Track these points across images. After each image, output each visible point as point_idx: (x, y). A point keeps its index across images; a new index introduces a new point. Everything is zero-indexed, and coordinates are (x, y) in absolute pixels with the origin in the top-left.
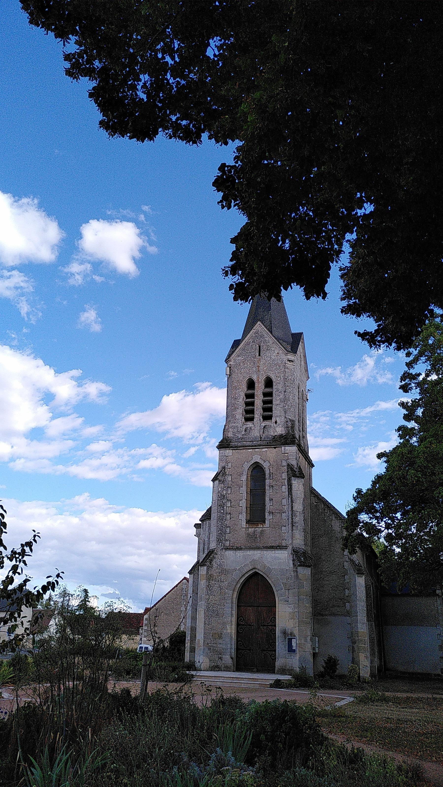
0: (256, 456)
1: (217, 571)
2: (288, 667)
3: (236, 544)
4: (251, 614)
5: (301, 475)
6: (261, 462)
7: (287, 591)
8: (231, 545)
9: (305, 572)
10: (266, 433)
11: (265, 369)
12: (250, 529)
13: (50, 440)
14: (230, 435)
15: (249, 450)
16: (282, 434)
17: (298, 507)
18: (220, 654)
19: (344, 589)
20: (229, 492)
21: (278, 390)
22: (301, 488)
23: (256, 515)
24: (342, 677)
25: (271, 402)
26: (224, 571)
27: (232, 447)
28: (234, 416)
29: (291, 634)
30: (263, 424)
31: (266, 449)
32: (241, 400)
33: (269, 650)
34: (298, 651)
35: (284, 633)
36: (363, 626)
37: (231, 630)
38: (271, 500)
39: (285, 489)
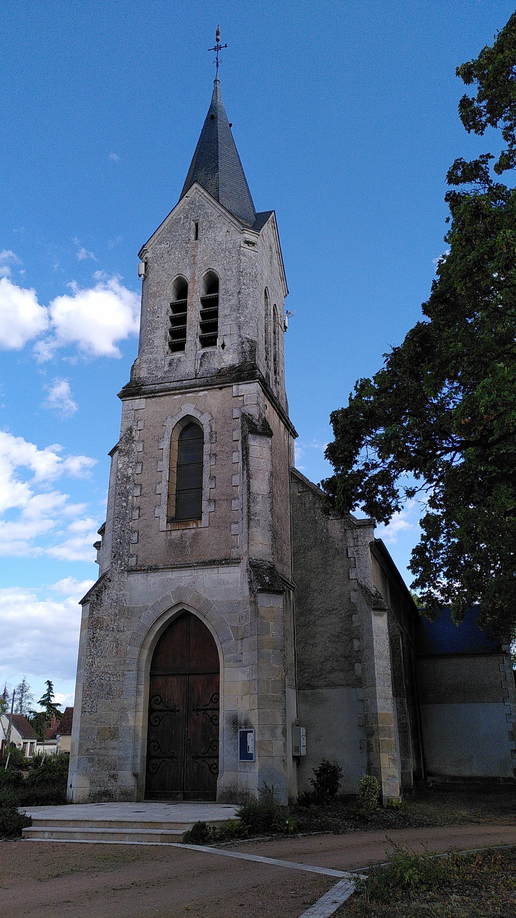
0: (187, 406)
1: (110, 611)
2: (239, 790)
3: (147, 561)
4: (174, 690)
5: (266, 431)
6: (197, 415)
7: (239, 641)
8: (139, 563)
9: (272, 604)
10: (206, 366)
11: (205, 258)
12: (174, 533)
13: (28, 520)
14: (143, 374)
15: (176, 397)
16: (234, 365)
17: (260, 486)
18: (113, 769)
19: (351, 640)
20: (139, 470)
21: (227, 292)
22: (266, 453)
23: (186, 504)
24: (349, 799)
25: (215, 314)
26: (125, 612)
27: (144, 393)
28: (150, 342)
29: (247, 724)
30: (202, 352)
31: (206, 392)
32: (163, 314)
33: (207, 757)
34: (257, 757)
35: (235, 722)
36: (385, 702)
37: (137, 720)
38: (213, 478)
39: (237, 457)
